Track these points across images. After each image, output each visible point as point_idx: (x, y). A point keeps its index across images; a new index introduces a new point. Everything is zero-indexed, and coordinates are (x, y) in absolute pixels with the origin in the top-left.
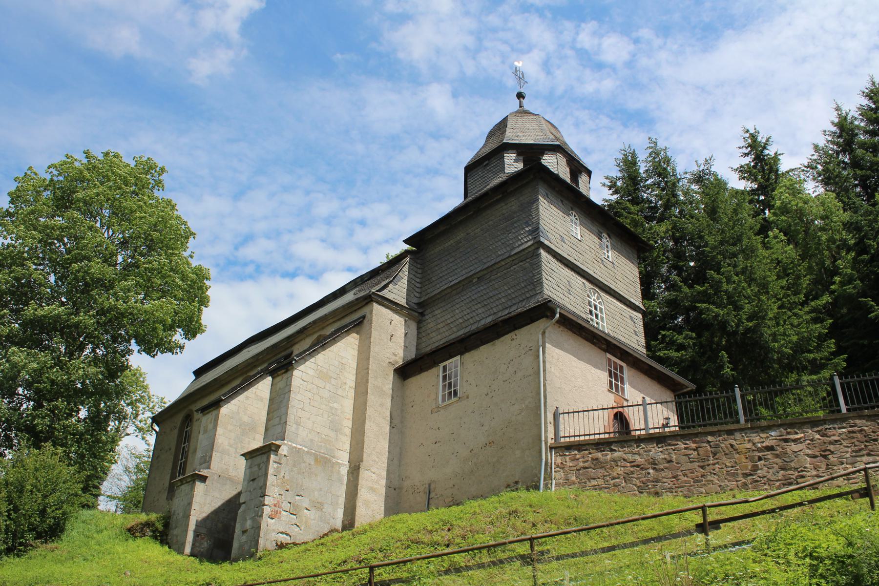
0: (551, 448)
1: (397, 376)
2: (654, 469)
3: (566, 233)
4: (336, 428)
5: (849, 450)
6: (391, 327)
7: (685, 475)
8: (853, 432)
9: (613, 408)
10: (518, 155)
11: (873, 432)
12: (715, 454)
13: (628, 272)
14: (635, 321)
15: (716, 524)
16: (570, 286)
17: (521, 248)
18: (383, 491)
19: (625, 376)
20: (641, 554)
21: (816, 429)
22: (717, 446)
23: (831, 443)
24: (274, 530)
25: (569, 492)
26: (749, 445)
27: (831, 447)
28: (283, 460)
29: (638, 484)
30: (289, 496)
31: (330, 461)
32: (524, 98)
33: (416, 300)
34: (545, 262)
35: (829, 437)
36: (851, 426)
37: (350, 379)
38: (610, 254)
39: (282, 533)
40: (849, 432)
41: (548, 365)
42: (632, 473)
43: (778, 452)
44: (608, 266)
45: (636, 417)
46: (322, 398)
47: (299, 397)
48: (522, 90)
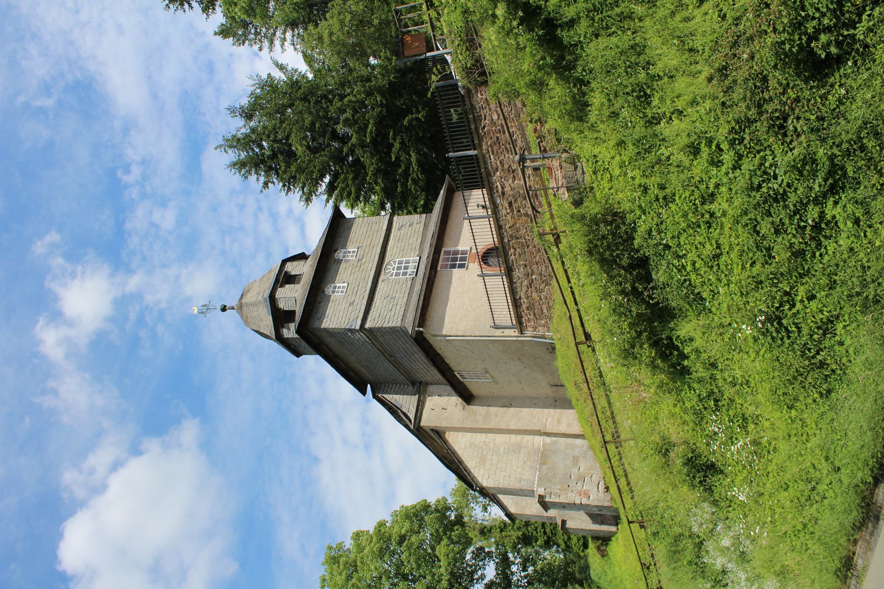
0: (522, 333)
1: (472, 403)
2: (532, 275)
3: (346, 298)
4: (518, 448)
5: (507, 155)
6: (436, 409)
7: (535, 257)
8: (493, 151)
9: (480, 265)
10: (283, 327)
11: (491, 138)
12: (517, 238)
13: (362, 230)
14: (401, 224)
15: (588, 336)
16: (388, 297)
17: (365, 337)
18: (558, 411)
19: (452, 249)
20: (642, 580)
21: (492, 174)
22: (511, 236)
23: (503, 166)
24: (597, 495)
25: (554, 325)
26: (509, 217)
27: (506, 167)
28: (548, 490)
29: (544, 285)
30: (572, 484)
31: (543, 452)
32: (225, 306)
33: (411, 388)
34: (375, 322)
35: (498, 167)
36: (488, 152)
37: (480, 437)
38: (352, 250)
39: (598, 488)
40: (493, 154)
41: (460, 333)
42: (536, 288)
43: (513, 200)
44: (362, 253)
45: (483, 244)
46: (498, 461)
47: (501, 480)
48: (219, 308)
